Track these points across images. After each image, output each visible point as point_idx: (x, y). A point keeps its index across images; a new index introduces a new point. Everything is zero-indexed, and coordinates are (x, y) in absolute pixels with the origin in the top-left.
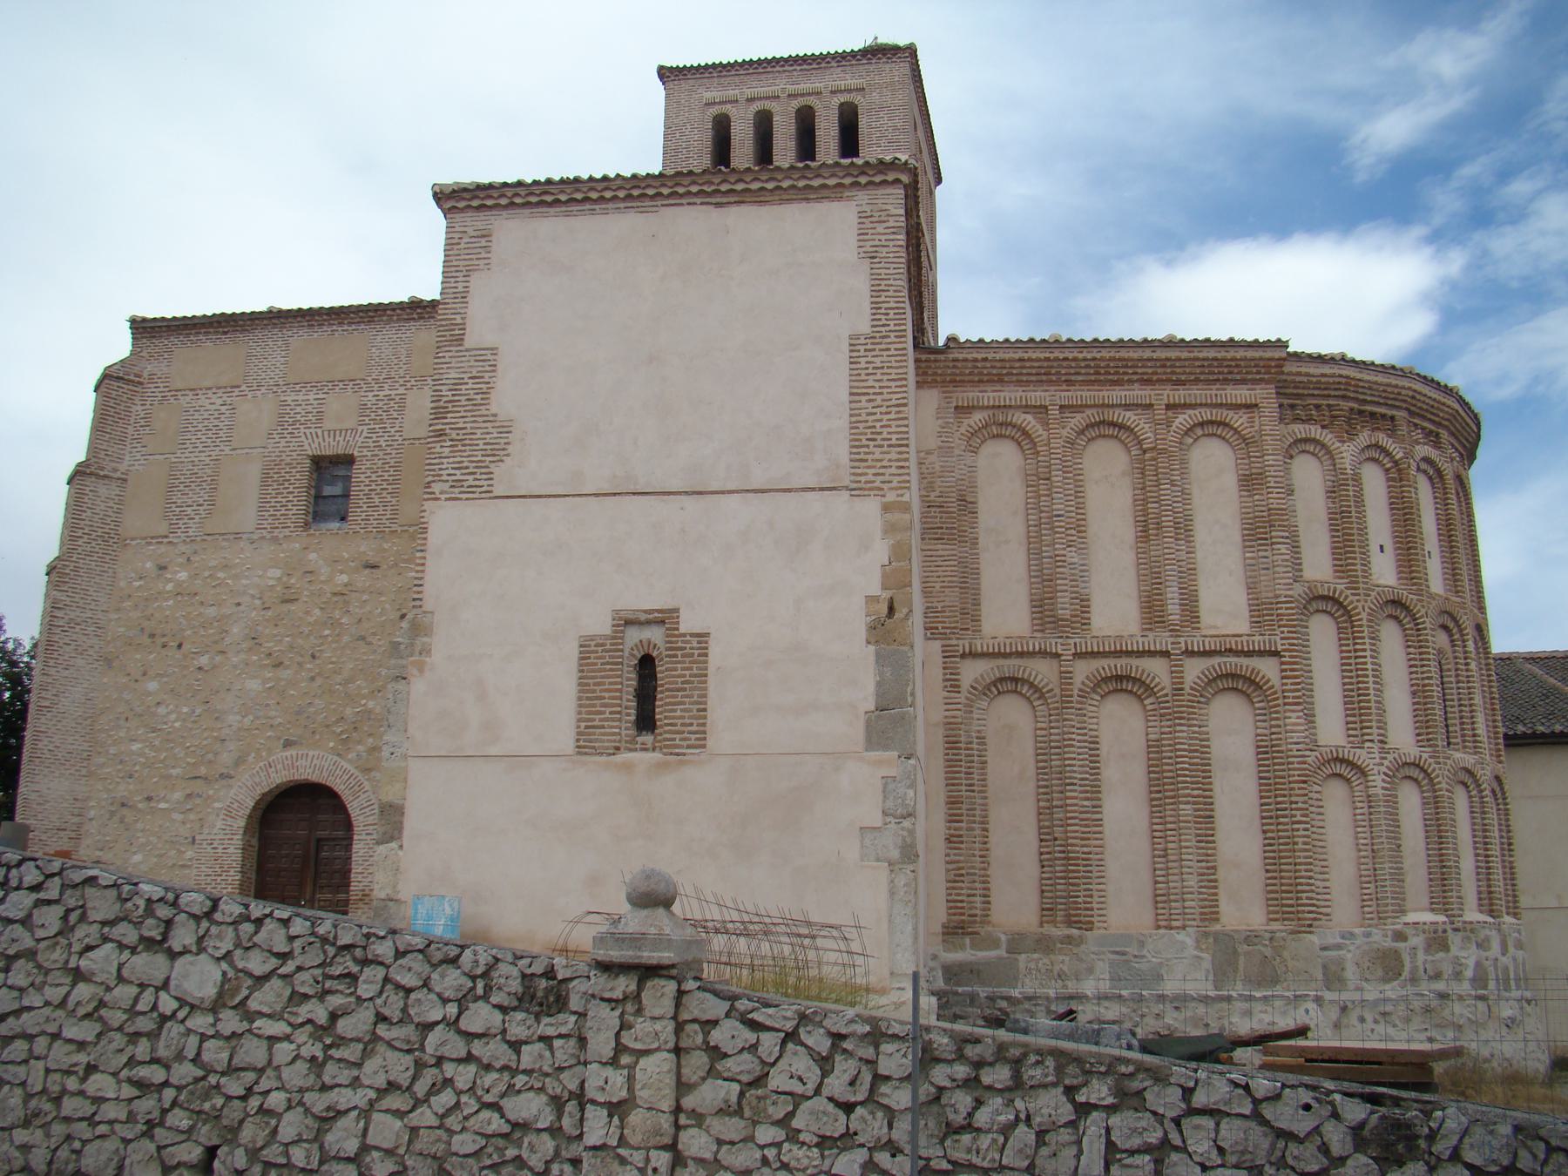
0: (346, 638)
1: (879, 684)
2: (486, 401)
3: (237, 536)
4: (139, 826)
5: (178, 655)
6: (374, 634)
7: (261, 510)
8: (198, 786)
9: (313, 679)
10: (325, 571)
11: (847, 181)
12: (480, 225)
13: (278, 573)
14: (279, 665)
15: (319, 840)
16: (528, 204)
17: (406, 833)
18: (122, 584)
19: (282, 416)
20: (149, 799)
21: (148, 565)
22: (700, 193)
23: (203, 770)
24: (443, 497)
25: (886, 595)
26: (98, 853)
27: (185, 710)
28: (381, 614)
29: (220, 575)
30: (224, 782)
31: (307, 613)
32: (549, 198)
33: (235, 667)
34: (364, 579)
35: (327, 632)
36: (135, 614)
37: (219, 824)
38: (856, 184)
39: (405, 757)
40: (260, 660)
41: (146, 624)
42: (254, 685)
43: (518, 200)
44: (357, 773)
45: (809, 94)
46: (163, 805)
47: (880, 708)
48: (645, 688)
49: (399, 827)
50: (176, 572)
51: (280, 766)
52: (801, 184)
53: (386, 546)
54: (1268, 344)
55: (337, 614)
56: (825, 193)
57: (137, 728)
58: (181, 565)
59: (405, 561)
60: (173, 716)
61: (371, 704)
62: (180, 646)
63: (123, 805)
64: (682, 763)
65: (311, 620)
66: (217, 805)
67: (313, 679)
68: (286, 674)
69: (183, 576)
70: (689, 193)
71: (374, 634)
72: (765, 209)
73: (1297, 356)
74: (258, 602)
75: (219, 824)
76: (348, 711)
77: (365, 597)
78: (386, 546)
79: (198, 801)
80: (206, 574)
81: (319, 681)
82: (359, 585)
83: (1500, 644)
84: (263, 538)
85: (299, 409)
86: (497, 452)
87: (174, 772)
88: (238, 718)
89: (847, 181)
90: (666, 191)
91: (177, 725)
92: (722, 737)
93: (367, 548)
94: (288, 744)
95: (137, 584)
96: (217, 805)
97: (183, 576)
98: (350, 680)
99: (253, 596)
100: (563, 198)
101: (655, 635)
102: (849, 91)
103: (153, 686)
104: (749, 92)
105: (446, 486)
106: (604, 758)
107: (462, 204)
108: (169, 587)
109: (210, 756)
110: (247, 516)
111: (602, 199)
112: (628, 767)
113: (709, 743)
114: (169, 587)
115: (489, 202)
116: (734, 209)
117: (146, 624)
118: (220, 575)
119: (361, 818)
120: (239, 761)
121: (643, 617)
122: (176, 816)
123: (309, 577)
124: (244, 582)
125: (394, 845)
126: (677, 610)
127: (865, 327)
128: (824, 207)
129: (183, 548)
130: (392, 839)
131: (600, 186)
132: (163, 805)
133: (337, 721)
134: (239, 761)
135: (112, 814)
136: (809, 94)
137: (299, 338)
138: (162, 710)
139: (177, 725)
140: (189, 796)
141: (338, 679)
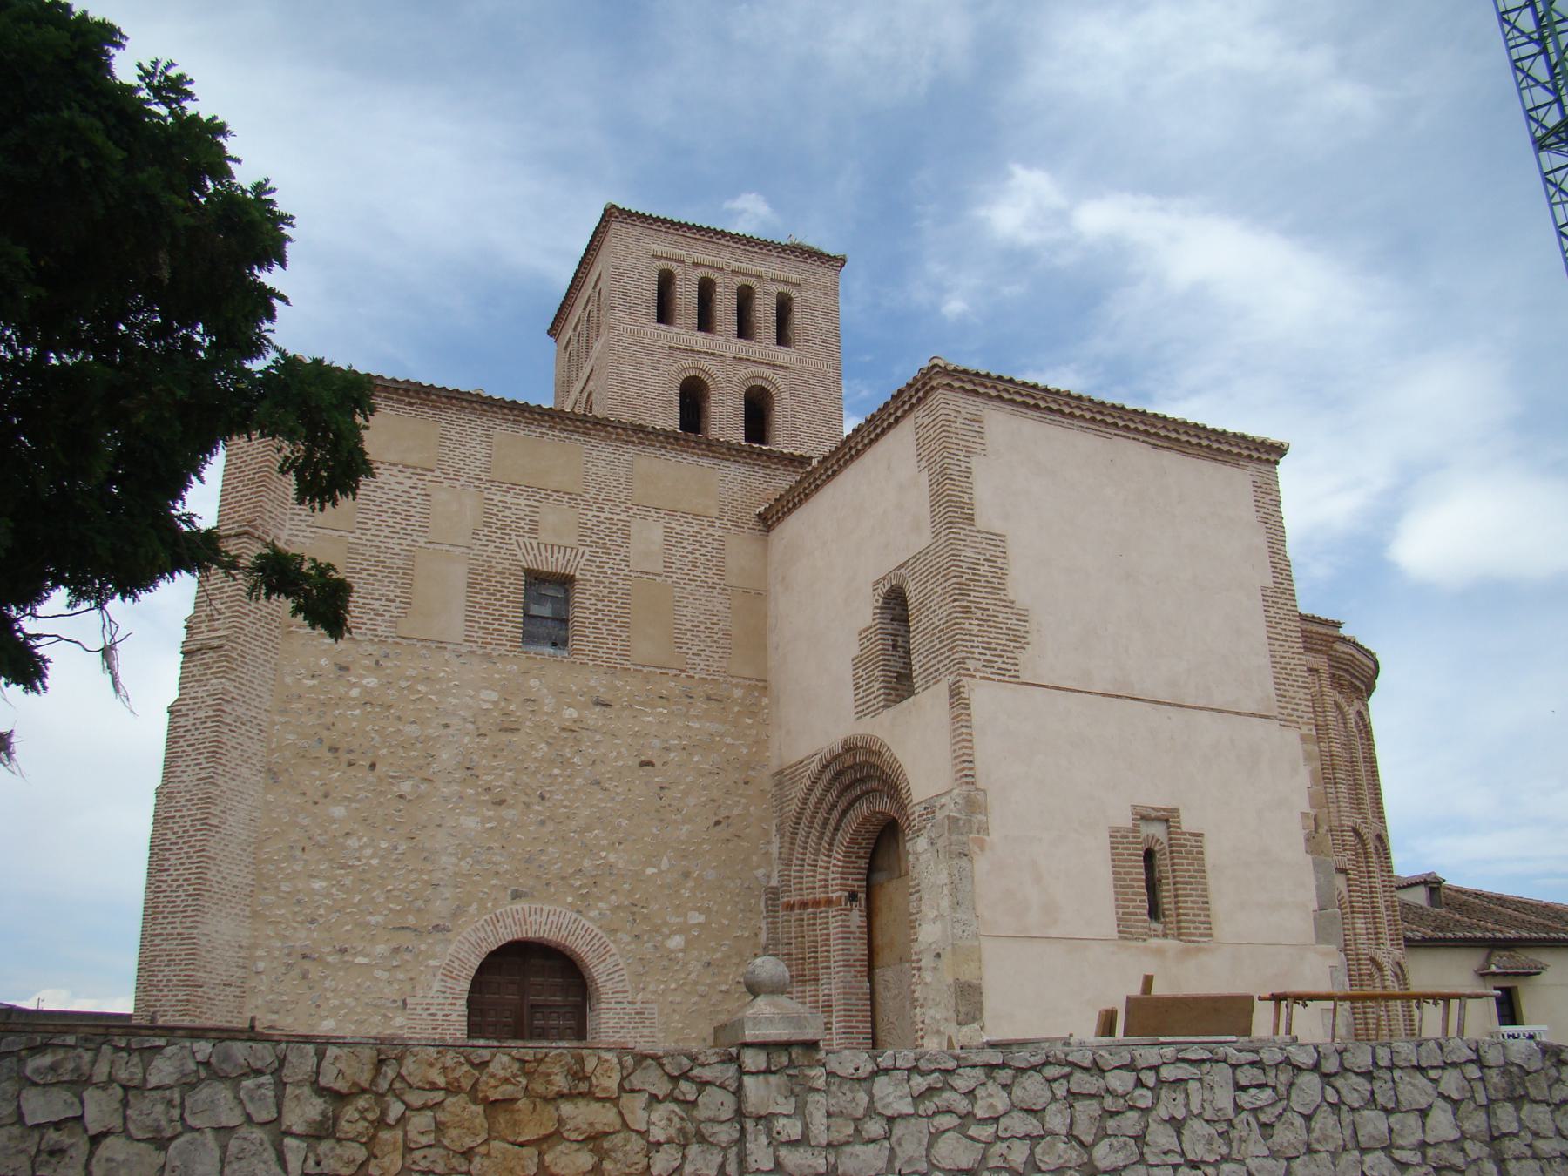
0: (579, 781)
1: (1318, 888)
2: (1002, 587)
3: (441, 645)
4: (327, 984)
5: (371, 777)
6: (610, 779)
7: (469, 619)
8: (406, 939)
9: (543, 823)
10: (549, 703)
11: (1245, 452)
12: (971, 409)
13: (494, 696)
14: (502, 802)
15: (532, 1006)
16: (1013, 401)
17: (987, 1014)
18: (288, 680)
19: (488, 515)
20: (343, 951)
21: (323, 662)
22: (1146, 432)
23: (411, 920)
24: (978, 675)
25: (1312, 812)
26: (274, 1017)
27: (384, 845)
28: (616, 759)
29: (421, 688)
30: (439, 936)
31: (532, 747)
32: (1032, 402)
33: (446, 799)
34: (594, 716)
35: (556, 771)
36: (312, 720)
37: (437, 986)
38: (1250, 457)
39: (976, 936)
40: (477, 794)
41: (325, 734)
42: (471, 823)
43: (1006, 396)
44: (601, 933)
45: (751, 275)
46: (360, 960)
47: (1321, 909)
48: (1158, 876)
49: (979, 1008)
50: (362, 677)
51: (509, 921)
52: (1215, 446)
53: (619, 684)
54: (1326, 623)
55: (568, 753)
56: (1227, 458)
57: (319, 862)
58: (367, 668)
59: (642, 704)
60: (368, 852)
61: (612, 858)
62: (373, 766)
63: (304, 957)
64: (1199, 950)
65: (539, 755)
66: (432, 963)
67: (543, 823)
68: (509, 813)
69: (371, 682)
70: (1136, 430)
71: (610, 779)
72: (1187, 459)
73: (1343, 639)
74: (471, 726)
75: (437, 986)
76: (586, 863)
77: (598, 737)
78: (619, 684)
79: (408, 957)
80: (404, 684)
81: (550, 826)
82: (591, 722)
83: (1405, 864)
84: (472, 652)
85: (508, 512)
86: (1019, 639)
87: (372, 919)
88: (454, 860)
89: (1245, 452)
90: (1121, 423)
91: (375, 862)
92: (1225, 928)
93: (598, 683)
94: (517, 895)
95: (309, 683)
96: (432, 963)
97: (371, 682)
98: (588, 828)
99: (465, 719)
100: (1043, 405)
101: (1158, 830)
102: (786, 283)
103: (339, 811)
104: (696, 257)
105: (979, 665)
106: (1141, 944)
107: (957, 384)
108: (354, 693)
109: (420, 903)
110: (453, 624)
111: (1071, 415)
112: (1160, 952)
113: (1215, 932)
114: (354, 693)
115: (981, 390)
116: (1166, 453)
117: (325, 734)
118: (421, 688)
119: (609, 984)
120: (457, 913)
121: (1153, 814)
122: (378, 973)
123: (532, 707)
124: (454, 701)
125: (976, 1026)
126: (1177, 810)
127: (1269, 582)
128: (1227, 470)
129: (370, 649)
130: (974, 1019)
131: (1074, 403)
132: (360, 960)
133: (575, 873)
134: (457, 913)
135: (289, 967)
136: (751, 275)
137: (504, 432)
138: (352, 842)
139: (375, 862)
140: (396, 950)
141: (573, 825)
